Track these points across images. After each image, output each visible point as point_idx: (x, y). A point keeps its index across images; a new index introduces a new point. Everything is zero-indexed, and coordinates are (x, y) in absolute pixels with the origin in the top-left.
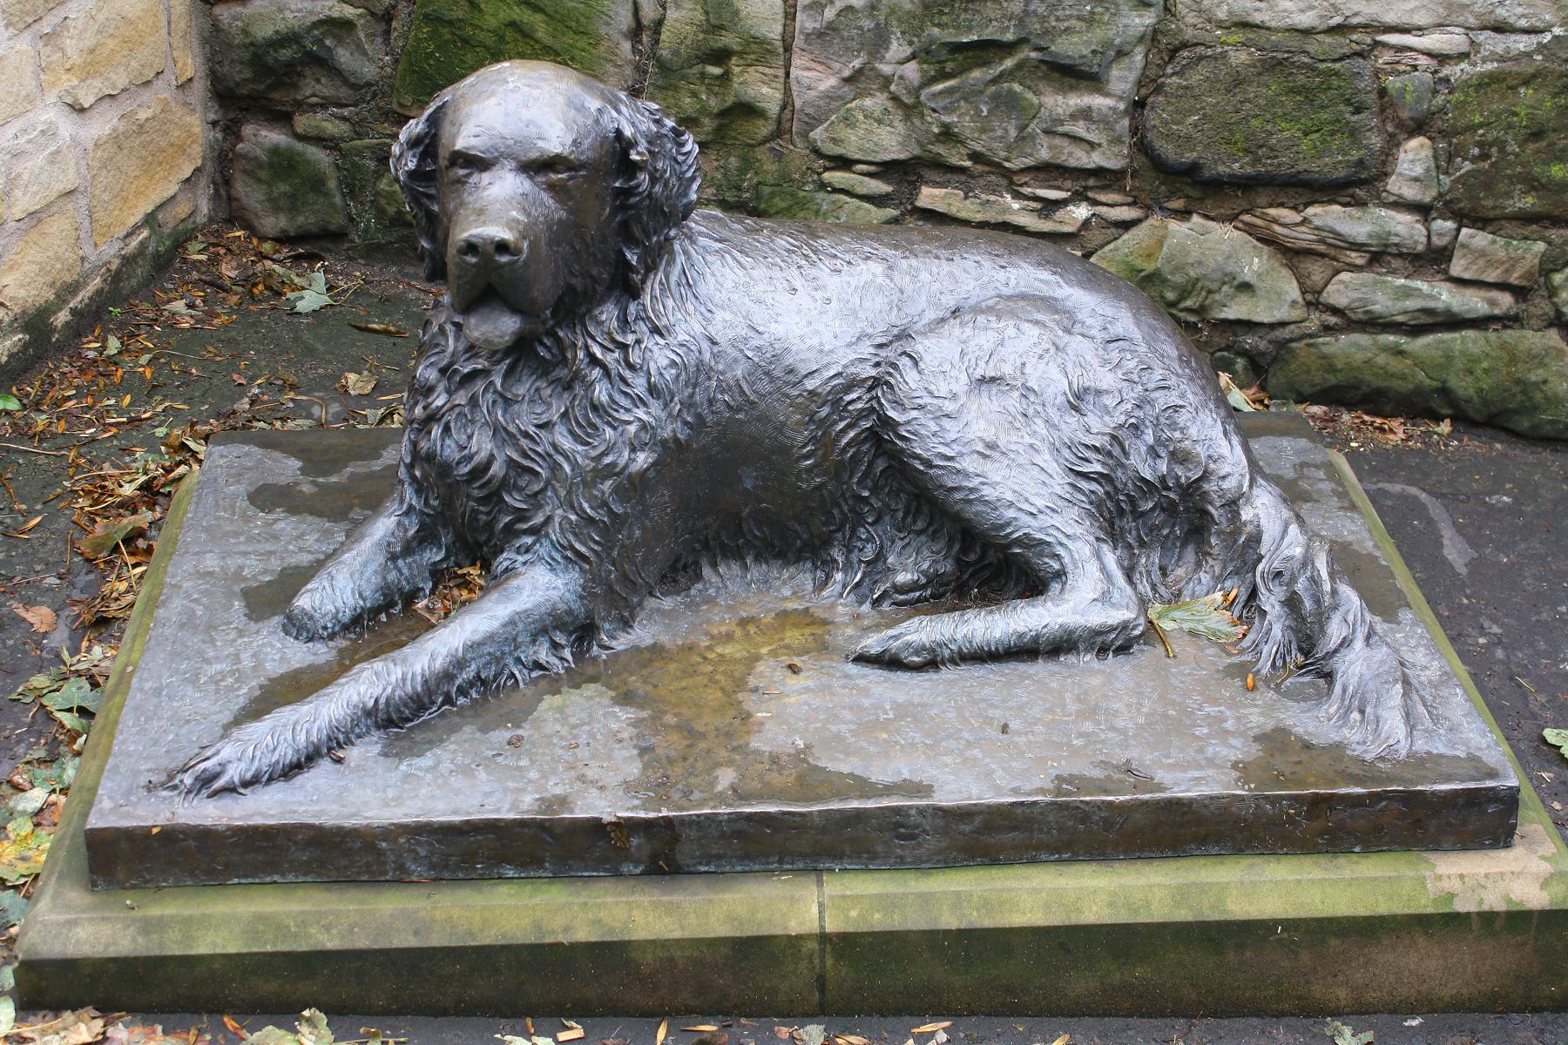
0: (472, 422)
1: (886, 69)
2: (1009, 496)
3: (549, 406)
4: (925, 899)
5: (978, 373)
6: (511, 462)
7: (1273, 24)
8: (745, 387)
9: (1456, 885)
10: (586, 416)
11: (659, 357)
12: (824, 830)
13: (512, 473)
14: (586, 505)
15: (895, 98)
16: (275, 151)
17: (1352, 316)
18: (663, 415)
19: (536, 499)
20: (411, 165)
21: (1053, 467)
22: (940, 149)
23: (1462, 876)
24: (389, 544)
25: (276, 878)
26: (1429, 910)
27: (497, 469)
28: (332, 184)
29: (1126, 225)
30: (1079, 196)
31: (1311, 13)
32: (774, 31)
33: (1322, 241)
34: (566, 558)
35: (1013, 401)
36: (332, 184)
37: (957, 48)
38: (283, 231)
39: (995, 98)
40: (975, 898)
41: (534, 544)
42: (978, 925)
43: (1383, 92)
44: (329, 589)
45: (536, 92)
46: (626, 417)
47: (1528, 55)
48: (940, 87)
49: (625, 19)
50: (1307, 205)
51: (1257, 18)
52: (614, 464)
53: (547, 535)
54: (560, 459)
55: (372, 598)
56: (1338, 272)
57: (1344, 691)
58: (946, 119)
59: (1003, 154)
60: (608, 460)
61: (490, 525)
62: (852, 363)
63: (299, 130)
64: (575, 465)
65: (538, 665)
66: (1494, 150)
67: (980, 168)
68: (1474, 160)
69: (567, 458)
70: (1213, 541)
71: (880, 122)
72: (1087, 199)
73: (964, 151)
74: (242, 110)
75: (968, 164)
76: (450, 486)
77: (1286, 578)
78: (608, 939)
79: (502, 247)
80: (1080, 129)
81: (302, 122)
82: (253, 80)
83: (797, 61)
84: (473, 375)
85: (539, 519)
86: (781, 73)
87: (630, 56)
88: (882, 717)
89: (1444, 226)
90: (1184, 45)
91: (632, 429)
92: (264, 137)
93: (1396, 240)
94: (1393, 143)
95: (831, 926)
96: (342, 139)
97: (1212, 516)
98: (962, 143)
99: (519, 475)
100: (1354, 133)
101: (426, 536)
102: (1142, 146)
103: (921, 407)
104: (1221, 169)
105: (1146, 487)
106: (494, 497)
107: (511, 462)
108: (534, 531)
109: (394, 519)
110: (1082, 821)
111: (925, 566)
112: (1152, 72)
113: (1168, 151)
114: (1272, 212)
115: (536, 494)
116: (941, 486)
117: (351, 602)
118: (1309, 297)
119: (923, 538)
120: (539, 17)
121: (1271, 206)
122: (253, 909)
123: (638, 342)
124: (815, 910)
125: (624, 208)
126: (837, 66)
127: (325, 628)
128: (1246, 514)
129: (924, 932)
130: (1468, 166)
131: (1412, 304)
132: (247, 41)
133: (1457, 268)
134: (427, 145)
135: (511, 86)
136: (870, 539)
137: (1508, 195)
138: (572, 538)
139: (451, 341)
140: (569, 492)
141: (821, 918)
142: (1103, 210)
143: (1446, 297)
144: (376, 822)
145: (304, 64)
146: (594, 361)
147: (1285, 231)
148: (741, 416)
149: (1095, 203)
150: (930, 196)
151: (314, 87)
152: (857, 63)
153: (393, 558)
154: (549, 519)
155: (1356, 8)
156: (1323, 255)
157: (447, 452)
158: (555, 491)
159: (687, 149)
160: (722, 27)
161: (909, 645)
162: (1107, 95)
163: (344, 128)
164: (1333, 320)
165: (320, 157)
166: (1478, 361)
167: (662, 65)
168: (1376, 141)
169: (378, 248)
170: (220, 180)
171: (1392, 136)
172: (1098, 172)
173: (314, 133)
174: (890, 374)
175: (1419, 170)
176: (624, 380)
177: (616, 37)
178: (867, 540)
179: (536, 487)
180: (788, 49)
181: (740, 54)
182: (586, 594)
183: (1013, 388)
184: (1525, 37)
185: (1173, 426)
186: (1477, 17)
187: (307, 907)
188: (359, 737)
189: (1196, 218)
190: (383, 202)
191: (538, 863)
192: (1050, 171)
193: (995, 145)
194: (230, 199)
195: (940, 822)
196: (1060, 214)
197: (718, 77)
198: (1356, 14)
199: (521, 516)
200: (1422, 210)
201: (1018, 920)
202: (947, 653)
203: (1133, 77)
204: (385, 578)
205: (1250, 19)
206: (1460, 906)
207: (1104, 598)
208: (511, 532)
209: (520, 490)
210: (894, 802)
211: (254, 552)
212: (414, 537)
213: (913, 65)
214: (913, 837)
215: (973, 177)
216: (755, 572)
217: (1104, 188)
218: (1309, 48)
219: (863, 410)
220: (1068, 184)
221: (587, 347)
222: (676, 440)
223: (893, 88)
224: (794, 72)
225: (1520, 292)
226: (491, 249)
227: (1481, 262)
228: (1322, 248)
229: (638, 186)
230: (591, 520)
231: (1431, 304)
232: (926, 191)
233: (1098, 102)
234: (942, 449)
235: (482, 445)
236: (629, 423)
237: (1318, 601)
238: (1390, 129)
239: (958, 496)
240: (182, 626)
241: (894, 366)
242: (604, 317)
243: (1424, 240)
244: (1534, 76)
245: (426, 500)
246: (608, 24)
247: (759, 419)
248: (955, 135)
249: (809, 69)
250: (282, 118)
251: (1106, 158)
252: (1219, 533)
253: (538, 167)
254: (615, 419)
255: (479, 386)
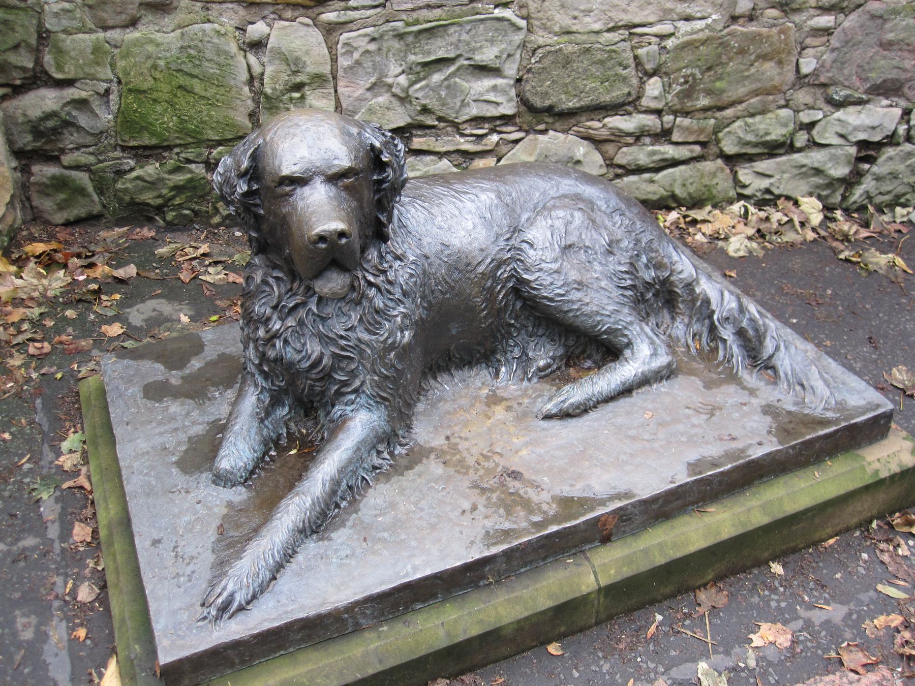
0: (303, 335)
1: (389, 80)
2: (595, 308)
3: (350, 317)
4: (646, 551)
5: (563, 244)
6: (335, 355)
7: (582, 31)
8: (448, 279)
9: (877, 465)
10: (373, 318)
11: (401, 274)
12: (586, 531)
13: (336, 361)
14: (383, 370)
15: (394, 95)
16: (53, 177)
17: (629, 168)
18: (413, 306)
19: (353, 374)
20: (245, 188)
21: (611, 287)
22: (421, 118)
23: (878, 460)
24: (257, 413)
25: (282, 652)
26: (870, 481)
27: (325, 360)
28: (90, 189)
29: (516, 142)
30: (493, 131)
31: (600, 23)
32: (326, 69)
33: (613, 134)
34: (377, 402)
35: (582, 255)
36: (90, 189)
37: (425, 65)
38: (67, 220)
39: (448, 87)
40: (669, 544)
41: (356, 398)
42: (674, 558)
43: (636, 57)
44: (236, 453)
45: (321, 129)
46: (395, 313)
47: (702, 30)
48: (418, 86)
49: (245, 76)
50: (604, 118)
51: (574, 28)
52: (394, 342)
53: (364, 392)
54: (363, 346)
55: (260, 449)
56: (620, 148)
57: (786, 375)
58: (424, 102)
59: (454, 115)
60: (390, 341)
61: (323, 393)
62: (498, 252)
63: (66, 164)
64: (372, 348)
65: (375, 468)
66: (690, 78)
67: (442, 124)
68: (681, 85)
69: (368, 345)
70: (681, 306)
71: (388, 109)
72: (496, 131)
73: (434, 117)
74: (28, 158)
75: (436, 123)
76: (293, 374)
77: (731, 320)
78: (488, 629)
79: (342, 234)
80: (491, 97)
81: (66, 159)
82: (34, 141)
83: (341, 84)
84: (296, 307)
85: (357, 383)
86: (332, 91)
87: (249, 94)
88: (578, 450)
89: (668, 118)
90: (539, 47)
91: (399, 319)
92: (44, 171)
93: (647, 128)
94: (642, 83)
95: (603, 582)
96: (92, 165)
97: (678, 293)
98: (433, 113)
99: (340, 361)
100: (625, 79)
101: (276, 401)
102: (523, 101)
103: (540, 270)
104: (564, 107)
105: (648, 285)
106: (327, 376)
107: (335, 355)
108: (356, 391)
109: (254, 398)
110: (709, 485)
111: (551, 354)
112: (524, 63)
113: (538, 103)
114: (589, 123)
115: (353, 371)
116: (561, 311)
117: (250, 456)
118: (608, 162)
119: (544, 338)
120: (196, 80)
121: (587, 121)
122: (278, 678)
123: (391, 267)
124: (592, 577)
125: (378, 191)
126: (362, 83)
127: (242, 477)
128: (698, 290)
129: (649, 570)
130: (679, 88)
131: (656, 158)
132: (26, 120)
133: (676, 137)
134: (254, 172)
135: (304, 128)
136: (516, 345)
137: (698, 99)
138: (377, 390)
139: (275, 289)
140: (372, 365)
141: (597, 580)
142: (503, 136)
143: (670, 151)
144: (339, 604)
145: (62, 127)
146: (371, 284)
147: (595, 132)
148: (448, 296)
149: (500, 132)
150: (418, 143)
151: (70, 139)
152: (373, 80)
153: (262, 421)
154: (363, 383)
155: (620, 17)
156: (612, 141)
157: (289, 355)
158: (363, 365)
159: (399, 148)
160: (298, 71)
161: (572, 404)
162: (504, 77)
163: (92, 159)
164: (620, 171)
165: (83, 178)
166: (687, 180)
167: (267, 97)
168: (635, 81)
169: (123, 218)
170: (24, 199)
171: (641, 78)
172: (503, 117)
173: (75, 164)
174: (520, 255)
175: (656, 93)
176: (389, 292)
177: (241, 85)
178: (515, 346)
179: (353, 367)
180: (335, 78)
181: (309, 84)
182: (390, 419)
183: (580, 248)
184: (699, 22)
185: (652, 250)
186: (677, 15)
187: (310, 666)
188: (298, 546)
189: (551, 132)
190: (120, 194)
191: (433, 596)
192: (478, 120)
193: (449, 112)
194: (32, 207)
195: (643, 508)
196: (485, 141)
197: (298, 99)
198: (620, 21)
199: (345, 384)
200: (658, 112)
201: (693, 548)
202: (592, 403)
203: (516, 66)
204: (262, 435)
205: (571, 30)
206: (884, 474)
207: (654, 354)
208: (339, 394)
209: (342, 369)
210: (618, 504)
211: (166, 432)
212: (269, 405)
213: (403, 77)
214: (630, 519)
215: (439, 129)
216: (458, 375)
217: (506, 124)
218: (600, 40)
219: (508, 277)
220: (486, 126)
221: (365, 277)
222: (421, 319)
223: (393, 90)
224: (340, 90)
225: (703, 144)
226: (335, 238)
227: (687, 133)
228: (612, 138)
229: (388, 177)
230: (387, 377)
231: (666, 156)
232: (415, 140)
233: (499, 81)
234: (558, 291)
235: (314, 348)
236: (397, 316)
237: (756, 330)
238: (640, 75)
239: (571, 315)
240: (148, 495)
241: (520, 249)
242: (370, 257)
243: (660, 126)
244: (706, 40)
245: (272, 382)
246: (235, 79)
247: (457, 295)
248: (429, 110)
249: (347, 87)
250: (54, 159)
251: (508, 109)
252: (683, 302)
253: (334, 178)
254: (389, 316)
255: (302, 313)
